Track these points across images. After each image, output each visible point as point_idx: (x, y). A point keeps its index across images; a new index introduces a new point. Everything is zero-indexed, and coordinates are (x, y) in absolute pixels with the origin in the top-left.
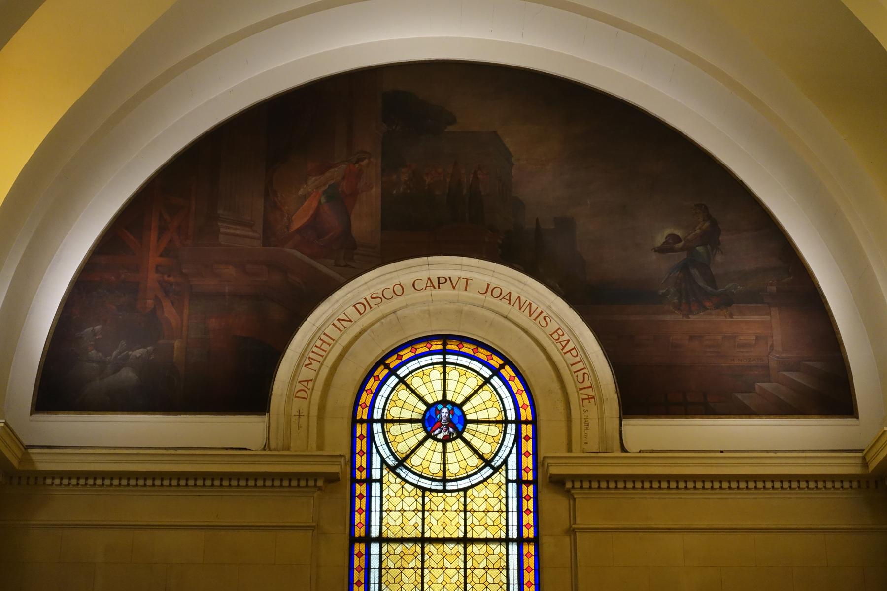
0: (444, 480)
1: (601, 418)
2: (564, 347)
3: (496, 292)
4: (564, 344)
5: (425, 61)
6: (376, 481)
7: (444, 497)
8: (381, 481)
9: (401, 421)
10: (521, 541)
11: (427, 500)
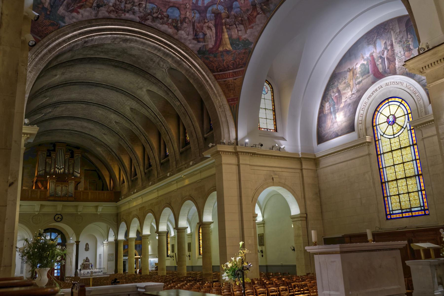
5: (224, 201)
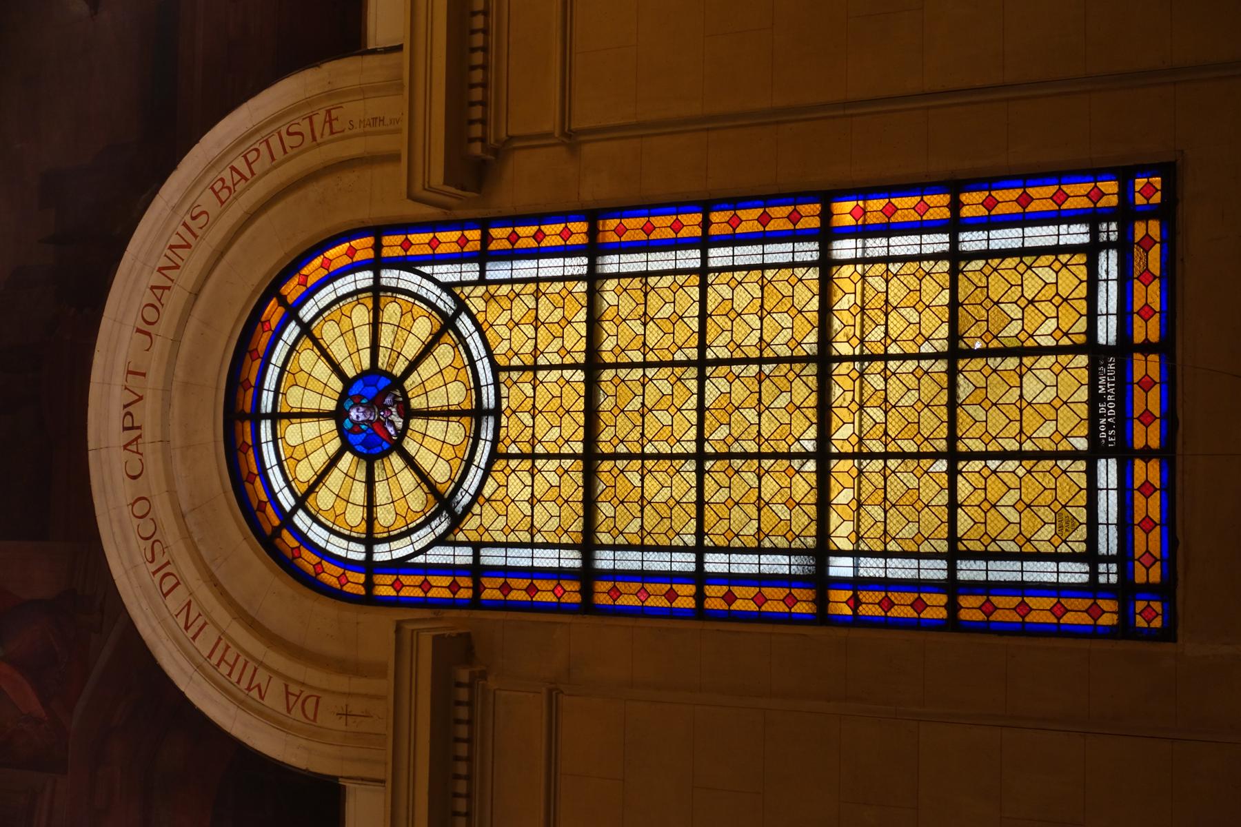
0: (477, 413)
1: (363, 92)
2: (243, 177)
3: (151, 314)
4: (237, 177)
6: (476, 556)
7: (508, 412)
8: (477, 546)
9: (370, 504)
10: (594, 249)
11: (513, 449)
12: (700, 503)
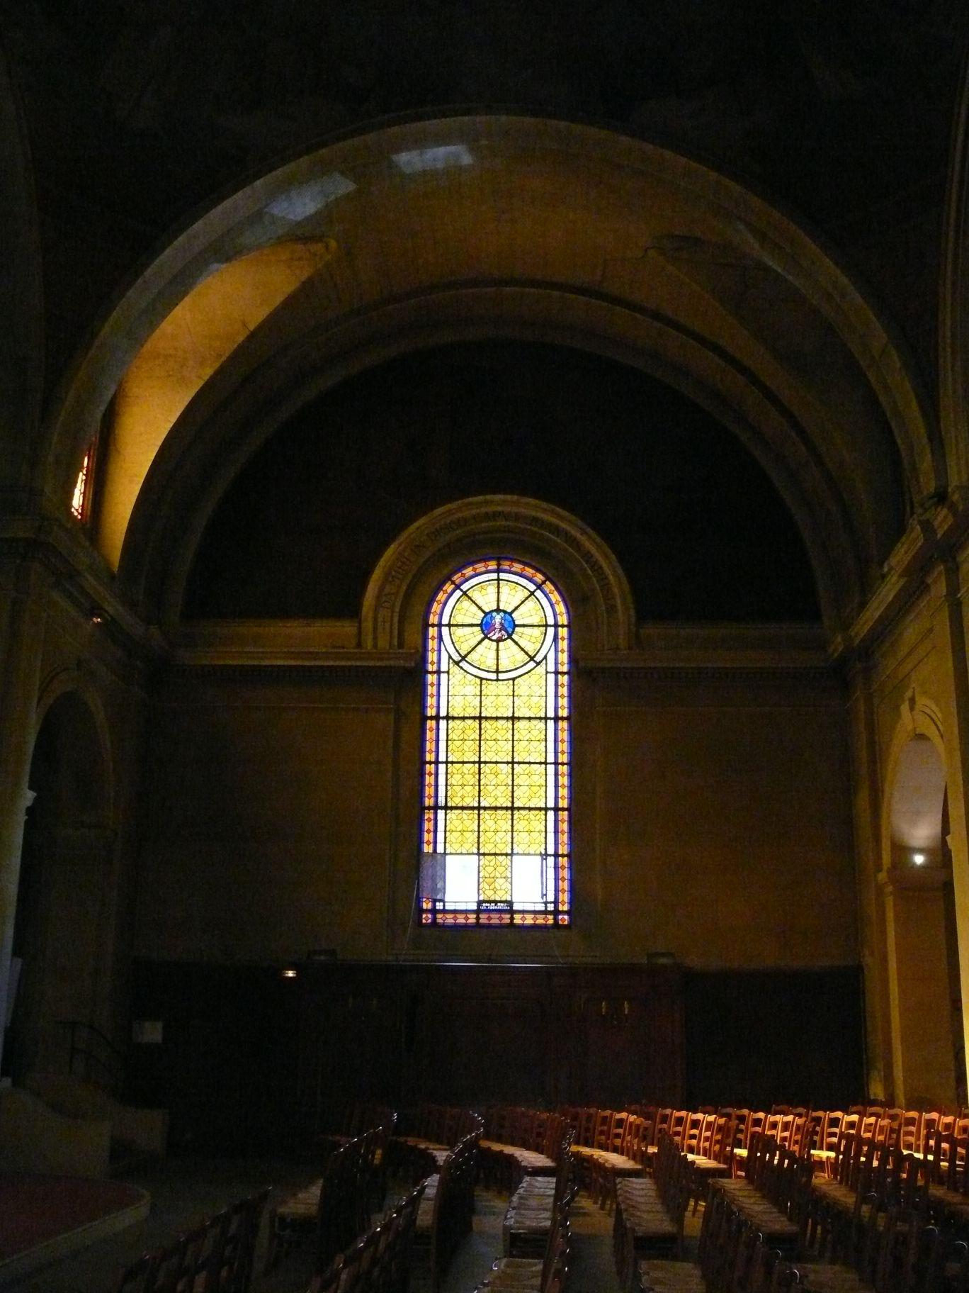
8: (448, 672)
12: (463, 763)
